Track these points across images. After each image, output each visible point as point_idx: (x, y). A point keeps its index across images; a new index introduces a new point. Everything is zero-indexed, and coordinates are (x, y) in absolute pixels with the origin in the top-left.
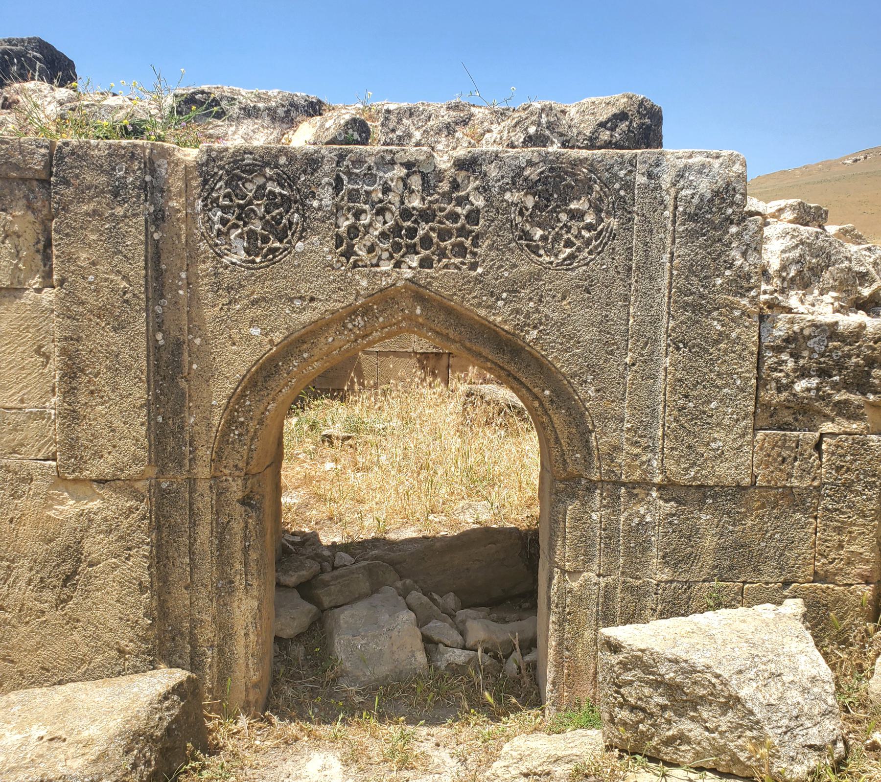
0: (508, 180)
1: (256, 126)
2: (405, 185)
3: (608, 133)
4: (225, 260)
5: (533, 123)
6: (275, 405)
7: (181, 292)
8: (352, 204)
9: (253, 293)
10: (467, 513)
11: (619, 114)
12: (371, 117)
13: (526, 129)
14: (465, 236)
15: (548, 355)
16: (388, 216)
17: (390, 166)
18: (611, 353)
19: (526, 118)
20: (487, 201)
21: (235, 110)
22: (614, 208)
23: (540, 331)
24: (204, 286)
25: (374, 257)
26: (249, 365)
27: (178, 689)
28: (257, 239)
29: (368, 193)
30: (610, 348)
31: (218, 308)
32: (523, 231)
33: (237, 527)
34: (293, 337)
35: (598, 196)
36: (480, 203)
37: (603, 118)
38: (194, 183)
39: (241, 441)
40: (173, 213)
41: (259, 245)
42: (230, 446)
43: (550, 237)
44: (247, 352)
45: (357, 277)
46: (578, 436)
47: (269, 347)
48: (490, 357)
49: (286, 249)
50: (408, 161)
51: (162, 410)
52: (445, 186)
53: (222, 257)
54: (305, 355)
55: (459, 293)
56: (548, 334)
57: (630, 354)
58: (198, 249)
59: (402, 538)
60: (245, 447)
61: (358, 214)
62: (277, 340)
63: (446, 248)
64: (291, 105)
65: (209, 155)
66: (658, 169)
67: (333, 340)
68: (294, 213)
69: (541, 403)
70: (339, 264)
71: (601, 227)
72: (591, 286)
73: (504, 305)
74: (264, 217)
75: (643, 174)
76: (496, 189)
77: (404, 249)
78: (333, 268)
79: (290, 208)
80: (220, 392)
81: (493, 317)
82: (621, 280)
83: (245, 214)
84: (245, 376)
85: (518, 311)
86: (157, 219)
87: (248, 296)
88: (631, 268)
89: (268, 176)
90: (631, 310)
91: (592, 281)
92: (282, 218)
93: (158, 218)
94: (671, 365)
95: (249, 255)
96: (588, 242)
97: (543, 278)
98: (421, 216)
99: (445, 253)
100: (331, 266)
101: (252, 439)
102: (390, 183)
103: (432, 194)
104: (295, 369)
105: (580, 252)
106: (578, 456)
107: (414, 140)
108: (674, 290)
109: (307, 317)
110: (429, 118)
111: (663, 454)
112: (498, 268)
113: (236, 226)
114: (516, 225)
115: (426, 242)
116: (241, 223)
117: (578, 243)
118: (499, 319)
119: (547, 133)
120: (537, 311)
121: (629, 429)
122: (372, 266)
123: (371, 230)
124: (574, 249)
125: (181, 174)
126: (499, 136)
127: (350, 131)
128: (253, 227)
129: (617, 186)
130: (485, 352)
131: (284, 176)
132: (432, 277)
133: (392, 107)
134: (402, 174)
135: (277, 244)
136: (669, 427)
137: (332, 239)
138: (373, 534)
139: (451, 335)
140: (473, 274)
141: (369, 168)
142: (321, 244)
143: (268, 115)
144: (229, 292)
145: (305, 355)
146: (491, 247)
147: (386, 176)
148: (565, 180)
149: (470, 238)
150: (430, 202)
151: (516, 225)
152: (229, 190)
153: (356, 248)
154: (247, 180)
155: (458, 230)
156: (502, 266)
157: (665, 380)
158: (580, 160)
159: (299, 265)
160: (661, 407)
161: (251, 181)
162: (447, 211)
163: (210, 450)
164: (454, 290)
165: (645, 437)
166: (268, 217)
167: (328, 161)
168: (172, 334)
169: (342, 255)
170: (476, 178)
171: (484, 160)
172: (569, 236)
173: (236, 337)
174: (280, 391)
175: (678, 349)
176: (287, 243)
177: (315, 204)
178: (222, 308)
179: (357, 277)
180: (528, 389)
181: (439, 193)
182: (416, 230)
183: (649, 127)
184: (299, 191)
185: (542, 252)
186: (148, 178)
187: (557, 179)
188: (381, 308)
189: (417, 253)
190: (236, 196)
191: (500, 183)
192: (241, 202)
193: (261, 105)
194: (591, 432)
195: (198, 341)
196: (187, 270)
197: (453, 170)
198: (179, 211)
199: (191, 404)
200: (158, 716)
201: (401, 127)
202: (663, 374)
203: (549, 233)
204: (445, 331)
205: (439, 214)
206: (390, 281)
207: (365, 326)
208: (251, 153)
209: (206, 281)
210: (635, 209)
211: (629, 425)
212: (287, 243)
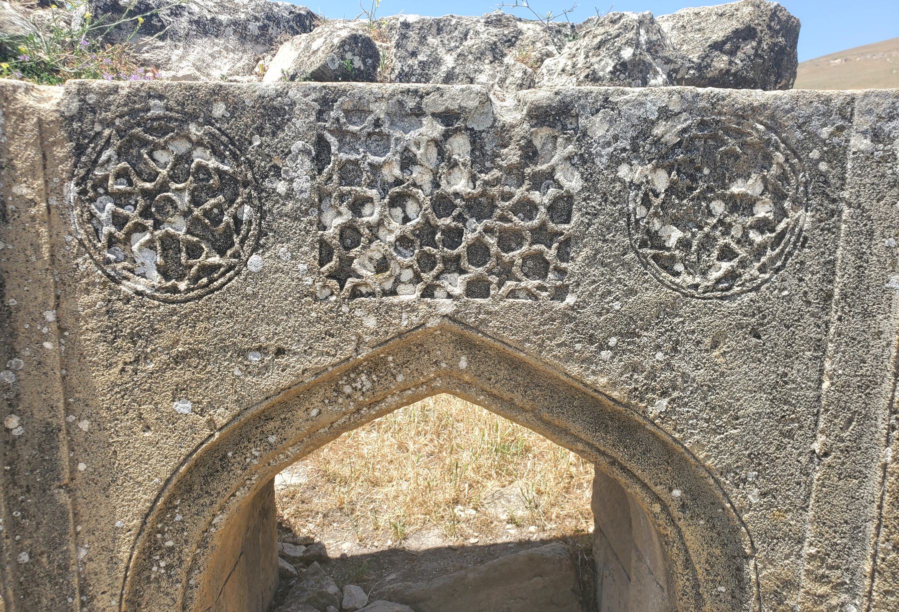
0: (626, 144)
1: (216, 48)
2: (441, 153)
3: (725, 58)
4: (126, 288)
5: (628, 43)
6: (225, 516)
7: (48, 345)
8: (348, 188)
9: (177, 342)
10: (499, 505)
11: (742, 31)
12: (380, 35)
14: (549, 241)
15: (684, 439)
16: (411, 208)
17: (414, 119)
19: (618, 36)
20: (586, 180)
21: (182, 24)
22: (806, 193)
23: (673, 400)
24: (89, 334)
25: (387, 279)
26: (173, 463)
28: (180, 251)
29: (375, 168)
30: (786, 426)
31: (116, 370)
32: (648, 232)
34: (248, 414)
35: (779, 172)
36: (573, 184)
37: (718, 36)
38: (60, 152)
39: (170, 576)
40: (22, 207)
41: (183, 261)
42: (153, 585)
43: (695, 243)
44: (171, 442)
46: (723, 560)
47: (207, 432)
48: (583, 436)
49: (230, 268)
51: (28, 542)
52: (512, 155)
53: (119, 283)
54: (272, 439)
55: (534, 338)
56: (686, 405)
57: (822, 438)
58: (75, 270)
59: (424, 547)
60: (179, 585)
61: (357, 206)
62: (221, 421)
63: (512, 263)
64: (268, 18)
65: (84, 100)
67: (320, 413)
68: (243, 203)
69: (665, 508)
70: (327, 292)
72: (762, 325)
74: (190, 211)
75: (864, 133)
76: (604, 160)
77: (440, 266)
78: (316, 299)
79: (237, 195)
81: (592, 378)
82: (812, 315)
83: (155, 207)
84: (168, 481)
85: (635, 368)
87: (167, 348)
88: (830, 296)
89: (194, 138)
90: (828, 365)
91: (764, 317)
92: (222, 213)
95: (167, 278)
96: (760, 251)
97: (681, 312)
98: (469, 207)
99: (510, 271)
100: (312, 295)
102: (414, 149)
104: (255, 462)
106: (723, 589)
107: (444, 69)
109: (272, 381)
110: (466, 35)
111: (870, 600)
112: (603, 296)
113: (140, 228)
114: (637, 221)
115: (479, 252)
116: (150, 222)
117: (742, 253)
118: (603, 380)
119: (649, 58)
120: (669, 366)
121: (812, 557)
122: (385, 293)
123: (382, 233)
125: (31, 135)
126: (570, 63)
127: (349, 56)
128: (171, 230)
129: (815, 154)
130: (576, 428)
131: (224, 138)
133: (411, 19)
135: (216, 259)
136: (883, 560)
137: (313, 248)
138: (389, 543)
139: (517, 401)
140: (559, 305)
141: (377, 123)
142: (293, 258)
143: (235, 31)
144: (134, 343)
145: (272, 439)
146: (591, 261)
147: (407, 136)
148: (724, 143)
149: (555, 245)
150: (486, 183)
151: (637, 221)
152: (124, 164)
153: (355, 265)
154: (157, 146)
155: (533, 230)
156: (610, 293)
157: (882, 484)
158: (753, 109)
159: (255, 295)
160: (871, 527)
161: (164, 148)
162: (516, 198)
163: (117, 598)
164: (526, 333)
165: (838, 568)
166: (197, 212)
167: (302, 110)
168: (37, 416)
169: (331, 276)
170: (568, 140)
171: (583, 107)
172: (728, 240)
173: (151, 418)
174: (234, 495)
176: (233, 256)
177: (281, 187)
178: (123, 370)
179: (358, 313)
180: (644, 486)
181: (500, 168)
182: (460, 233)
183: (782, 50)
184: (251, 164)
185: (679, 267)
187: (711, 142)
188: (400, 360)
189: (462, 272)
190: (139, 174)
191: (611, 149)
192: (148, 185)
193: (224, 18)
194: (747, 557)
195: (85, 425)
196: (57, 306)
197: (526, 126)
198: (32, 203)
199: (79, 528)
201: (425, 49)
202: (880, 473)
204: (507, 395)
205: (501, 204)
206: (415, 320)
207: (373, 388)
208: (161, 97)
209: (92, 323)
210: (846, 194)
211: (813, 551)
212: (233, 256)
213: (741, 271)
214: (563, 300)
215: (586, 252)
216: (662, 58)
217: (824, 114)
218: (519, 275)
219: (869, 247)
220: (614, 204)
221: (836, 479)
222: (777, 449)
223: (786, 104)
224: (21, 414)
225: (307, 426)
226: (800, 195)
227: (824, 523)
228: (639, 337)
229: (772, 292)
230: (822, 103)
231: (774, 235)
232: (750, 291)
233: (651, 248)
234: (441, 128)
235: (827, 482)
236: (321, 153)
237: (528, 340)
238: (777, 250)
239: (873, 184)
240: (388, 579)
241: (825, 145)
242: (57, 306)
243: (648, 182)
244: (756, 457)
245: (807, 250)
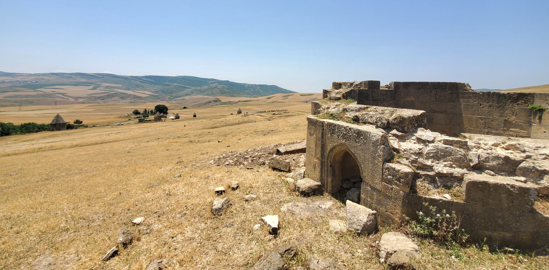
80: (329, 149)
93: (323, 129)
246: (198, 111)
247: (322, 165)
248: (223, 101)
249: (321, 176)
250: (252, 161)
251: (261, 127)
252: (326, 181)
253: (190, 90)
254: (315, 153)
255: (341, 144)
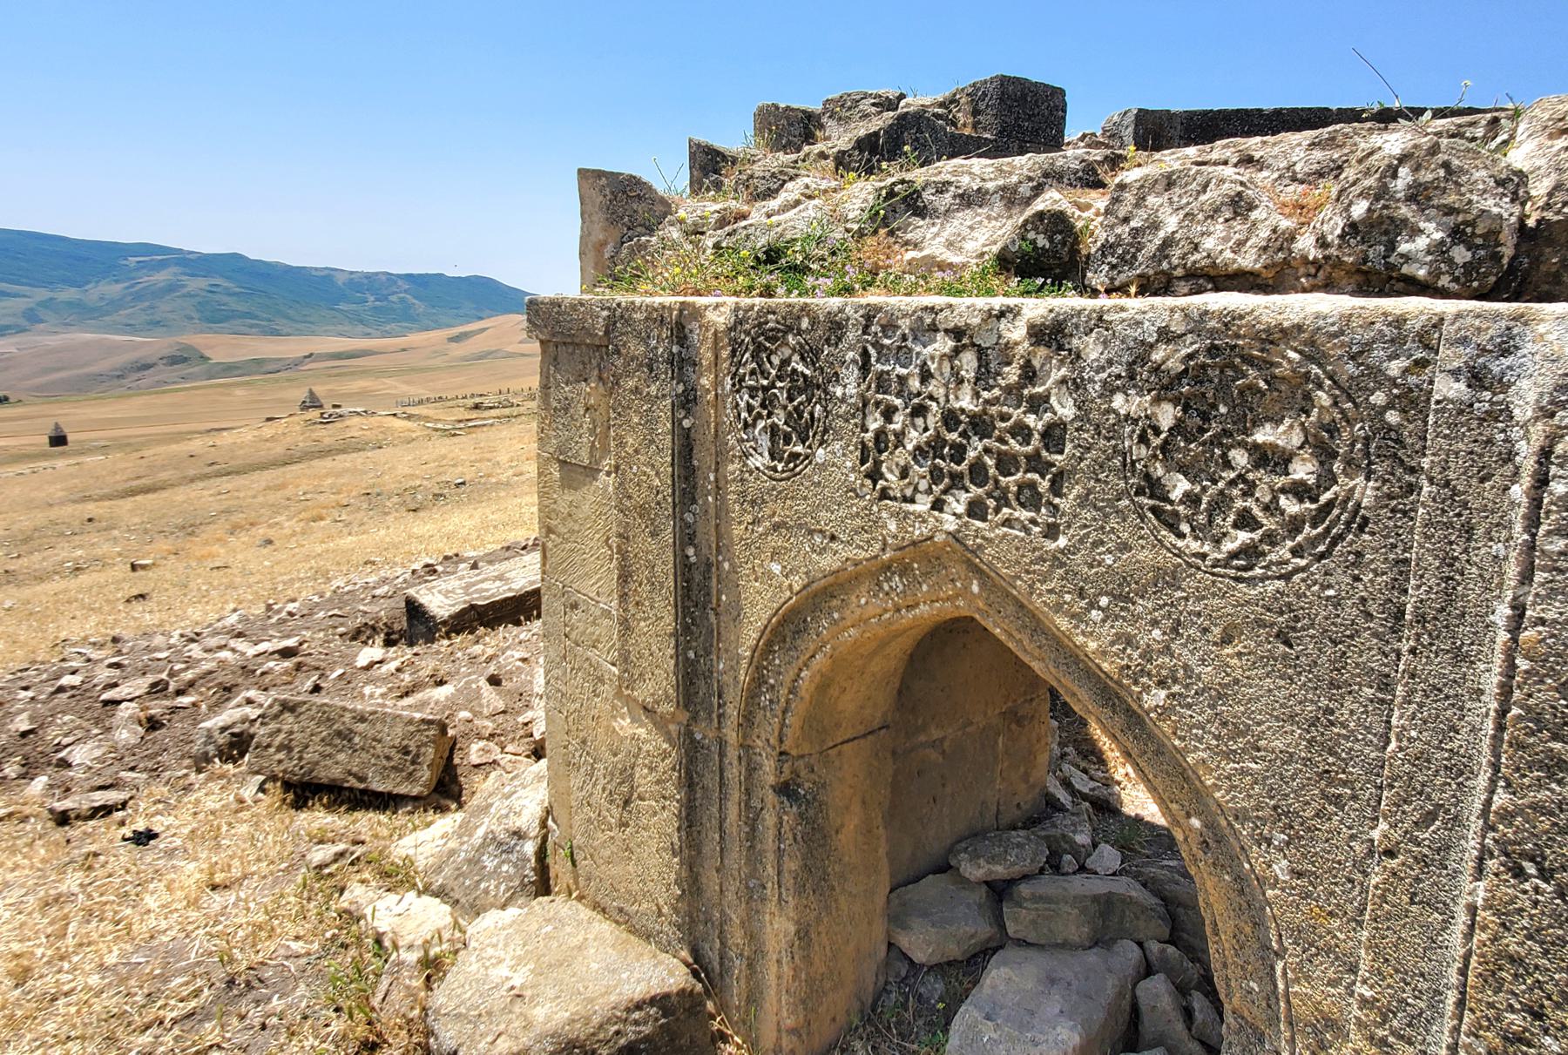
13: (1347, 209)
18: (1337, 801)
20: (1079, 408)
23: (1173, 696)
27: (661, 1002)
29: (902, 380)
32: (1147, 477)
33: (769, 819)
45: (884, 515)
47: (788, 594)
50: (956, 327)
52: (1012, 374)
56: (1189, 706)
57: (1383, 826)
61: (888, 414)
66: (1506, 362)
71: (1328, 495)
72: (1294, 629)
73: (1104, 621)
75: (1455, 374)
76: (1097, 387)
80: (749, 634)
81: (1081, 638)
82: (1376, 635)
86: (688, 401)
88: (1401, 613)
91: (1297, 619)
93: (688, 401)
94: (1488, 906)
96: (1295, 525)
100: (854, 490)
101: (784, 712)
103: (993, 387)
105: (1273, 544)
108: (1515, 711)
109: (827, 562)
112: (1096, 544)
118: (1092, 645)
120: (1167, 650)
122: (905, 499)
124: (1257, 535)
127: (1031, 235)
129: (1379, 398)
132: (983, 538)
134: (947, 350)
140: (1051, 546)
141: (904, 338)
146: (1083, 501)
147: (925, 351)
148: (1245, 376)
150: (987, 402)
151: (1133, 463)
156: (1102, 543)
158: (1283, 331)
170: (1062, 362)
171: (1077, 326)
172: (1250, 503)
175: (1519, 873)
177: (839, 392)
185: (1185, 528)
186: (675, 349)
188: (923, 570)
191: (1104, 375)
195: (726, 565)
197: (1026, 344)
200: (616, 1028)
203: (1204, 489)
210: (1426, 463)
213: (1267, 548)
214: (1056, 539)
215: (1078, 490)
216: (1438, 207)
217: (1392, 341)
218: (1014, 503)
219: (1466, 551)
220: (1109, 439)
221: (1406, 899)
222: (1317, 815)
223: (1333, 324)
224: (695, 547)
225: (858, 611)
226: (1357, 455)
227: (1387, 960)
228: (1134, 604)
229: (1309, 587)
230: (1390, 325)
231: (1314, 506)
232: (1279, 578)
233: (1151, 497)
234: (951, 344)
235: (1390, 897)
236: (865, 367)
237: (1019, 578)
238: (1320, 529)
239: (1471, 453)
240: (1165, 863)
241: (1396, 386)
242: (717, 470)
243: (1147, 417)
244: (1286, 814)
245: (1366, 537)
246: (75, 416)
247: (690, 782)
248: (218, 356)
249: (692, 885)
250: (153, 724)
251: (403, 469)
252: (737, 937)
253: (21, 304)
254: (625, 659)
255: (915, 560)
